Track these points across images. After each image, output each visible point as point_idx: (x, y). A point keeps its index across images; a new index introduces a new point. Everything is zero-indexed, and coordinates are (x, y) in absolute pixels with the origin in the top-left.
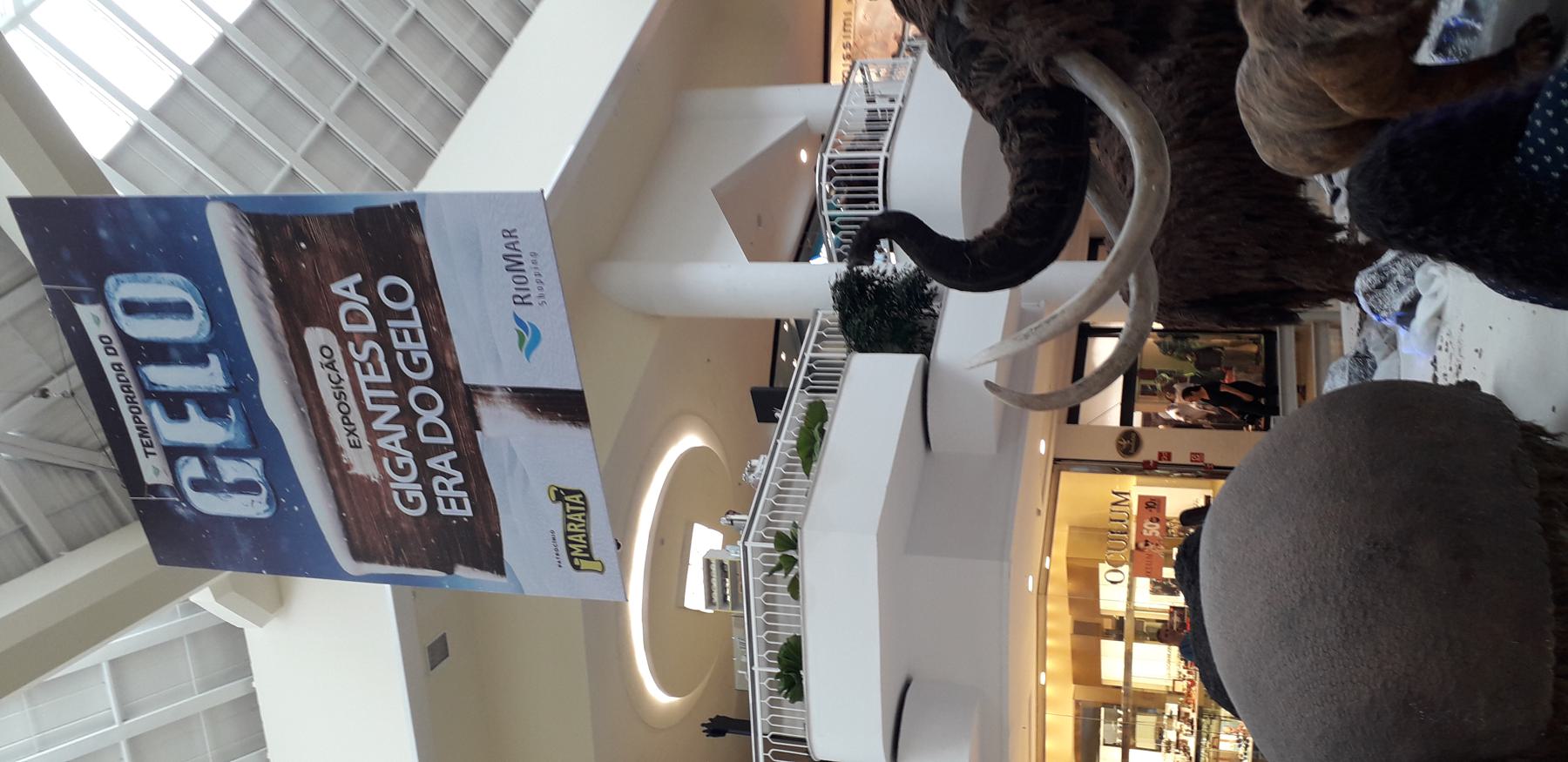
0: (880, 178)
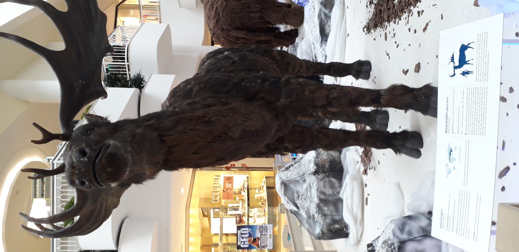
0: (126, 51)
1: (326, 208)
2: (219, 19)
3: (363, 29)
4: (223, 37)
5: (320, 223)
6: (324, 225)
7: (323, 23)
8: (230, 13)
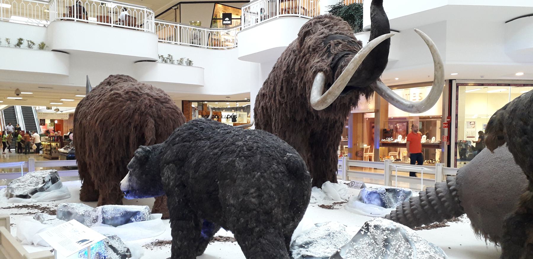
2: (162, 103)
4: (140, 107)
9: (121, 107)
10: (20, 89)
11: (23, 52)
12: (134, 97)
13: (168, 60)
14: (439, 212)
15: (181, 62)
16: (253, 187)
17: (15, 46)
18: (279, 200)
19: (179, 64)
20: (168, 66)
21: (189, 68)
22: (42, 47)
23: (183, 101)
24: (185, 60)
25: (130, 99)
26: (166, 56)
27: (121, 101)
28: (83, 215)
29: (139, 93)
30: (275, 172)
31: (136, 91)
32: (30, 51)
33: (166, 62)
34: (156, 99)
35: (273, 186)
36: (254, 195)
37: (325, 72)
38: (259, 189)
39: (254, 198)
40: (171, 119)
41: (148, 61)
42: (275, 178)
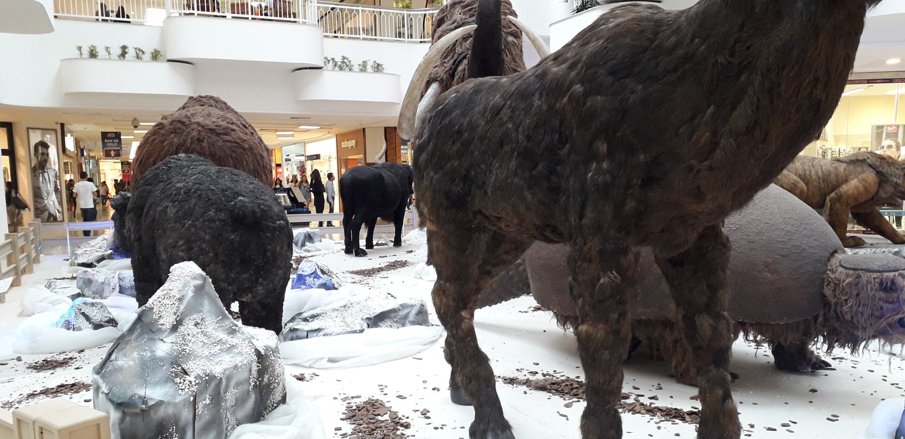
1: (208, 402)
2: (218, 134)
3: (283, 400)
4: (185, 141)
5: (174, 396)
6: (175, 405)
7: (393, 315)
8: (234, 155)
9: (163, 142)
10: (138, 119)
11: (130, 65)
12: (179, 129)
13: (344, 65)
14: (516, 279)
15: (363, 68)
16: (182, 239)
17: (119, 57)
18: (216, 254)
19: (361, 70)
20: (345, 75)
21: (378, 76)
22: (156, 56)
23: (385, 128)
24: (370, 64)
25: (174, 131)
26: (339, 59)
27: (164, 135)
28: (103, 283)
29: (188, 122)
30: (212, 220)
31: (184, 120)
32: (139, 64)
33: (341, 69)
34: (211, 130)
35: (207, 237)
36: (183, 248)
37: (441, 82)
38: (188, 242)
39: (182, 251)
40: (231, 156)
41: (310, 68)
42: (210, 228)
